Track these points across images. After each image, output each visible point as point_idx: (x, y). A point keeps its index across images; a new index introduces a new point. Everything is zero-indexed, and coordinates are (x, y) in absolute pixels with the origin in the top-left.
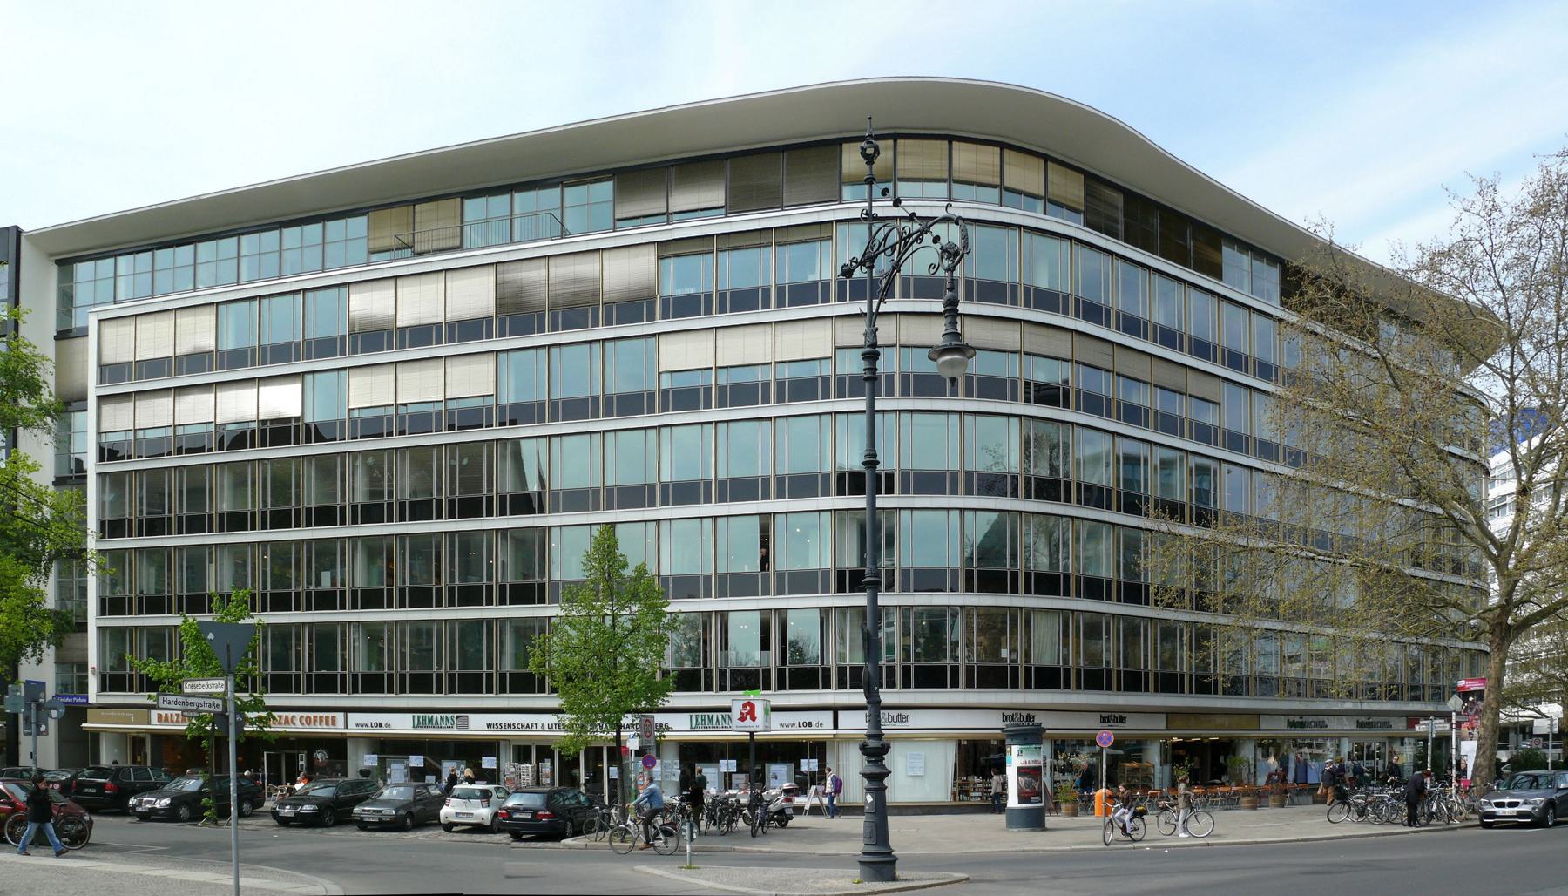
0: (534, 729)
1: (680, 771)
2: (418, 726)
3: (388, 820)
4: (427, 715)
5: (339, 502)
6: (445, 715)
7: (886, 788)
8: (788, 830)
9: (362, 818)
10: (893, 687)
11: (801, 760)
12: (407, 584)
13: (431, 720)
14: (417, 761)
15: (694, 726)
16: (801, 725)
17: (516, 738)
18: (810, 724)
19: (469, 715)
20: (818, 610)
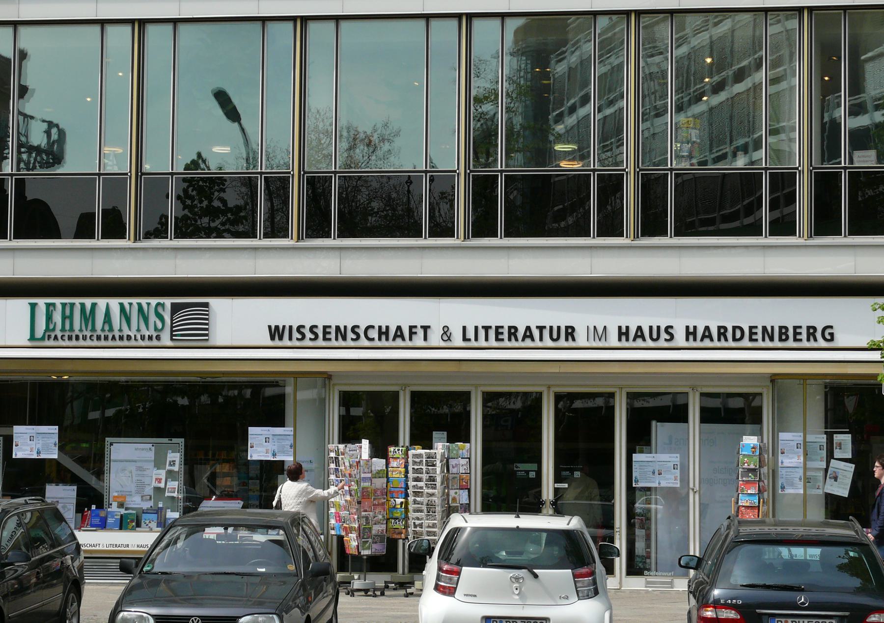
0: (419, 341)
1: (851, 467)
2: (49, 332)
4: (77, 301)
6: (135, 301)
7: (518, 527)
10: (449, 232)
13: (88, 317)
15: (40, 332)
16: (471, 334)
17: (555, 369)
18: (570, 332)
19: (216, 303)
20: (128, 29)
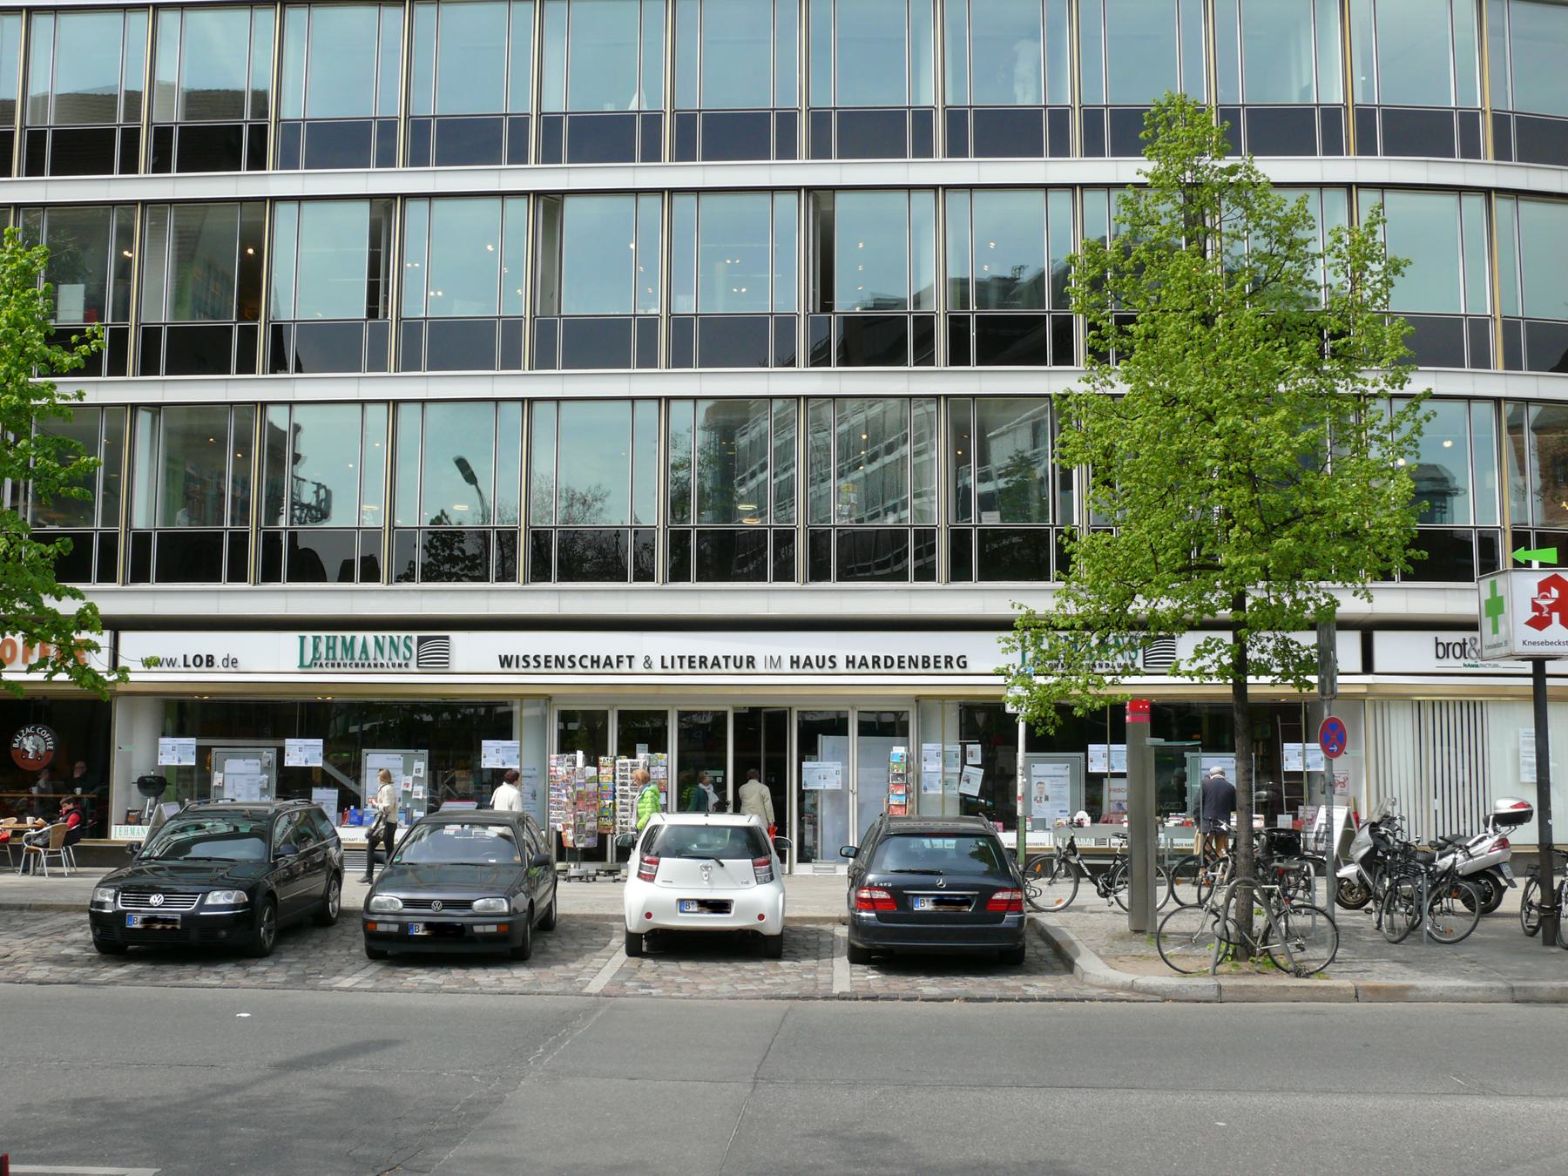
0: (625, 668)
3: (493, 929)
5: (120, 119)
6: (387, 634)
8: (1500, 921)
9: (404, 927)
10: (376, 579)
11: (484, 743)
12: (973, 307)
13: (348, 648)
14: (304, 752)
15: (307, 662)
16: (190, 661)
17: (737, 691)
18: (751, 661)
